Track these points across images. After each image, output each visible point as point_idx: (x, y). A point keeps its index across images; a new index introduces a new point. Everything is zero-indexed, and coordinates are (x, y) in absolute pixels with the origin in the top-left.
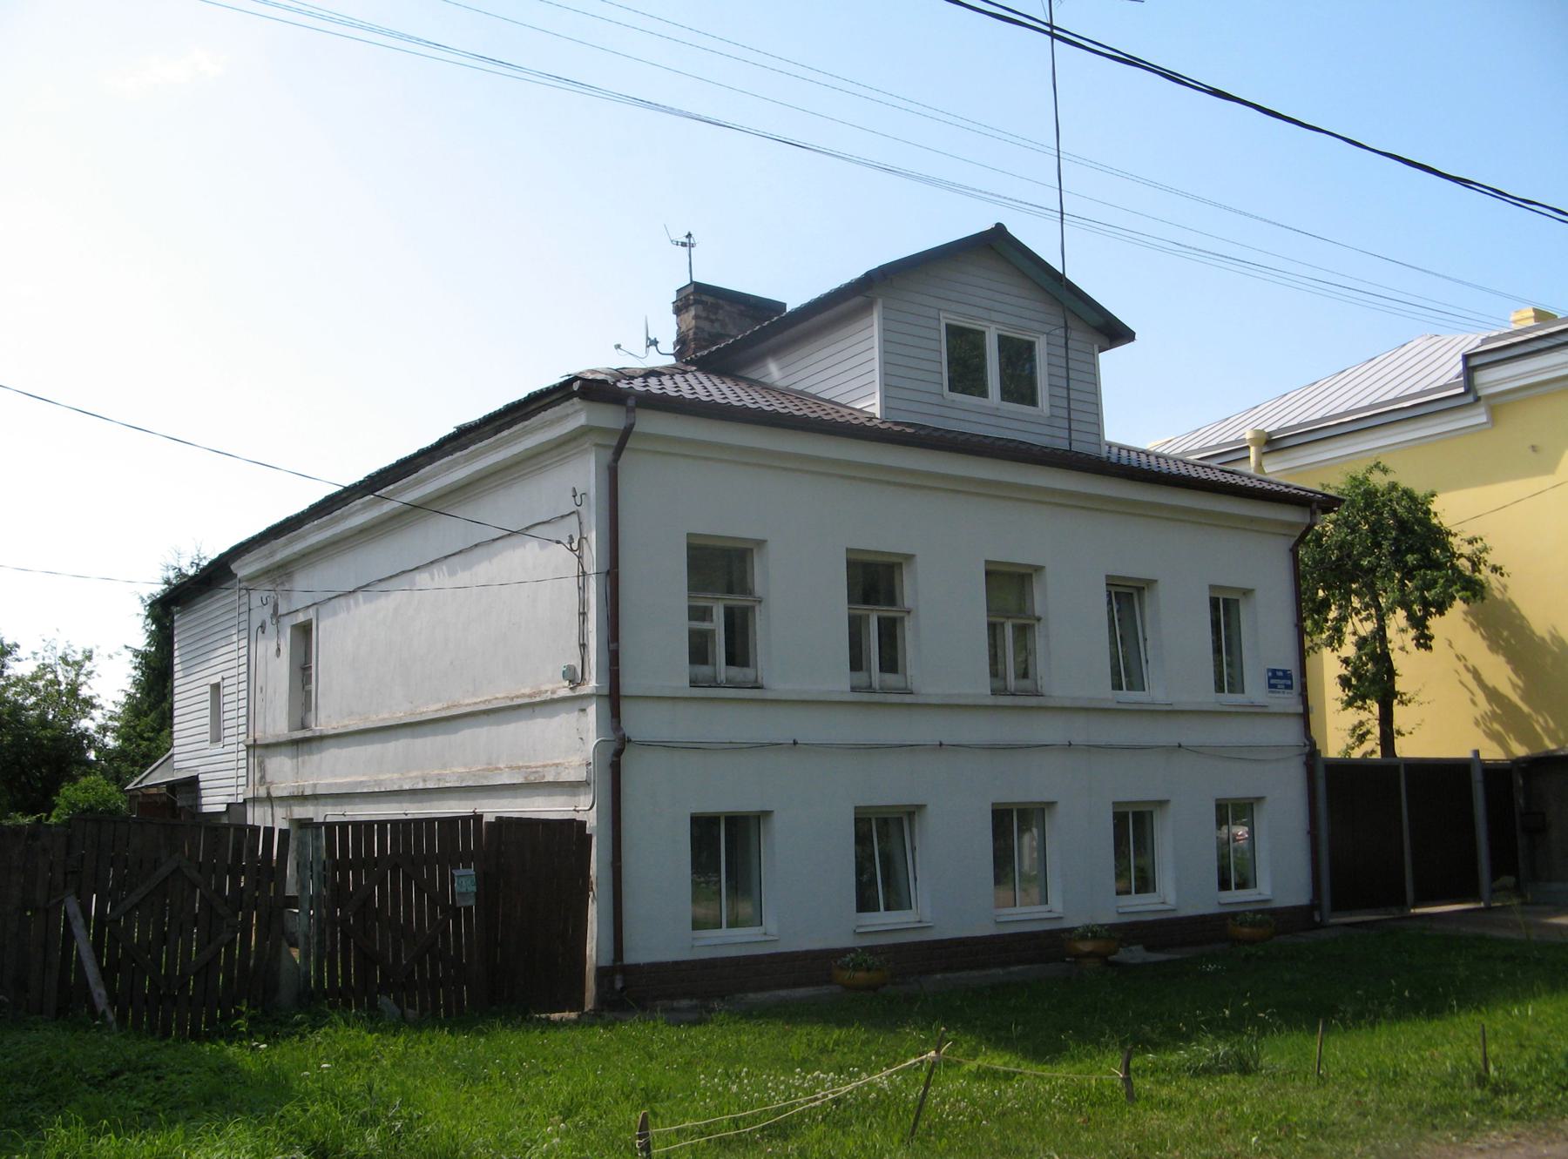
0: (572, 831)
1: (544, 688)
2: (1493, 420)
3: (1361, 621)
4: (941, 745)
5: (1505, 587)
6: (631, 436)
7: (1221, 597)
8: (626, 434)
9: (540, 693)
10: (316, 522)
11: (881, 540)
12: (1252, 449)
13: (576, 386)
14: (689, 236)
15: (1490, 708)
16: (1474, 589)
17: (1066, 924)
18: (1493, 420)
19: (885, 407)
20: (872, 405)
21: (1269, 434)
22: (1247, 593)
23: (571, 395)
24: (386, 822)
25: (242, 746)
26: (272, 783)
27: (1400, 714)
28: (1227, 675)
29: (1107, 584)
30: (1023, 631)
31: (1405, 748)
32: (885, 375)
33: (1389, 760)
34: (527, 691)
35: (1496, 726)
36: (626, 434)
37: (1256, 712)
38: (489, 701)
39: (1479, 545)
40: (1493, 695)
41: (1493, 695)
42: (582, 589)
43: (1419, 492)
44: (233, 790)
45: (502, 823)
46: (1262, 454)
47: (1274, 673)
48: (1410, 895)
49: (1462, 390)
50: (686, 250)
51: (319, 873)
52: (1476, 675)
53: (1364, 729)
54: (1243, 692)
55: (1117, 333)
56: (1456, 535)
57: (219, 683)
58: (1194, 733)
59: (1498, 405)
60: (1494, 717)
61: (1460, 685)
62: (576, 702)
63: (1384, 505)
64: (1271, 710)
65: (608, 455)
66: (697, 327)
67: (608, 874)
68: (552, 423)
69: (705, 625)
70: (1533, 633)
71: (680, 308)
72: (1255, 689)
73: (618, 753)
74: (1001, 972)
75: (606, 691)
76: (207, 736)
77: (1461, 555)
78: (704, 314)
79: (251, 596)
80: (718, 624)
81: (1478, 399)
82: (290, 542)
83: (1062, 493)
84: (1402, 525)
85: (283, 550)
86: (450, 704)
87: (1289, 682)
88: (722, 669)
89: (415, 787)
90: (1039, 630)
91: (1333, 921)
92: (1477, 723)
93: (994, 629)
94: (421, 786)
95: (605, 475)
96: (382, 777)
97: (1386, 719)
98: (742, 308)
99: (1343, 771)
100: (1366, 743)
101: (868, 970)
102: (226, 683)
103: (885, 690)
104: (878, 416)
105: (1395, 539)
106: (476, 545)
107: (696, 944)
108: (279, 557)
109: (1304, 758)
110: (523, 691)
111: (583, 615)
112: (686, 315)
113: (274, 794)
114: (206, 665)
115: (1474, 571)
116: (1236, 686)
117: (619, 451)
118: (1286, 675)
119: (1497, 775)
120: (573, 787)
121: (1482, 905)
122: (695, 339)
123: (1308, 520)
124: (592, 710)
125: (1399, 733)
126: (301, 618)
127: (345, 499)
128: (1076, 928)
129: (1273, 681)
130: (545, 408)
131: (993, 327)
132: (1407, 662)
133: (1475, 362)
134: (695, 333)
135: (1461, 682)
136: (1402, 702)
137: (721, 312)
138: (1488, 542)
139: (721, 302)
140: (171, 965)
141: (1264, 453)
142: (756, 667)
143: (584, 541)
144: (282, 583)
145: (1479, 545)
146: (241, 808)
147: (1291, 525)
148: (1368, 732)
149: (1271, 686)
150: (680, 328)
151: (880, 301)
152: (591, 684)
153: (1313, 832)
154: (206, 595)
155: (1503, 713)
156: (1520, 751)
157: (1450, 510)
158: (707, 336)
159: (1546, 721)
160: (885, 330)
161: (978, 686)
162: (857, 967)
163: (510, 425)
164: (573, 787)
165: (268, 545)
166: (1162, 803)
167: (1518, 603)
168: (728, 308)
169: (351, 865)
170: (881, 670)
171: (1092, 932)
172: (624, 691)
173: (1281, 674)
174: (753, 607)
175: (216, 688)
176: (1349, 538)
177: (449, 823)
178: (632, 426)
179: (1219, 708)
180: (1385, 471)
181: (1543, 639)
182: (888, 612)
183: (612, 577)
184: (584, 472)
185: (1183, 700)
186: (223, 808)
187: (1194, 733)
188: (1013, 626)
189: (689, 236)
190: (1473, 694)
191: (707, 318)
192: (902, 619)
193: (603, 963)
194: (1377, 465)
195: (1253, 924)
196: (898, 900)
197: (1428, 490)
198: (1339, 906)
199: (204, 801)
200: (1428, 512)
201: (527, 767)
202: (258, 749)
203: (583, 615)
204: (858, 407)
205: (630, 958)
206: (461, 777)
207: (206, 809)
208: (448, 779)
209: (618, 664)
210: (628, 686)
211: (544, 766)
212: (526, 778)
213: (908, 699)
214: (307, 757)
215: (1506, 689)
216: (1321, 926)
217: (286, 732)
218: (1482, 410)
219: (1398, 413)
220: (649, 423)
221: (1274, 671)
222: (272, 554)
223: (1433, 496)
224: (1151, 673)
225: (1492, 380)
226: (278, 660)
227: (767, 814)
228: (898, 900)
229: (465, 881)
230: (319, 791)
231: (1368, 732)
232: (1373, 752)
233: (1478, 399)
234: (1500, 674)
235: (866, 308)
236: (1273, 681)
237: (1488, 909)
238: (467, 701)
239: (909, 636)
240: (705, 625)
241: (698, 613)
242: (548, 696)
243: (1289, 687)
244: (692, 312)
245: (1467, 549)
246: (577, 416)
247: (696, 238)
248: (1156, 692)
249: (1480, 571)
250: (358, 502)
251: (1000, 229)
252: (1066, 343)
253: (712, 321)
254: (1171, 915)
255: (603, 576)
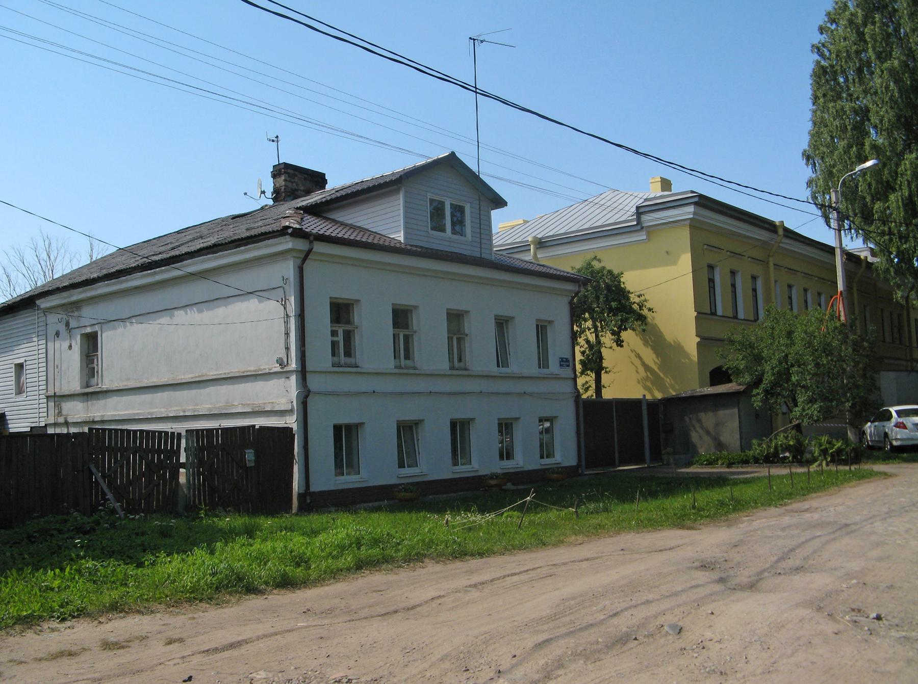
0: (288, 431)
1: (262, 367)
2: (649, 238)
3: (591, 333)
4: (525, 393)
5: (654, 318)
6: (311, 254)
7: (540, 324)
8: (309, 252)
9: (261, 370)
10: (106, 282)
11: (405, 300)
12: (532, 246)
13: (290, 231)
14: (277, 137)
15: (645, 374)
16: (642, 318)
17: (480, 473)
18: (649, 238)
19: (405, 238)
20: (400, 237)
21: (540, 239)
22: (551, 322)
23: (287, 234)
24: (204, 430)
25: (43, 396)
26: (67, 415)
27: (604, 377)
28: (543, 362)
29: (495, 319)
30: (459, 340)
31: (607, 394)
32: (406, 223)
33: (599, 399)
34: (252, 369)
35: (649, 384)
36: (309, 252)
37: (555, 377)
38: (228, 373)
39: (642, 298)
40: (647, 368)
41: (647, 368)
42: (286, 323)
43: (616, 272)
44: (37, 420)
45: (262, 429)
46: (536, 249)
47: (562, 360)
48: (617, 461)
49: (635, 223)
50: (275, 143)
51: (194, 453)
52: (638, 356)
53: (588, 385)
54: (548, 368)
55: (499, 202)
56: (632, 293)
57: (23, 363)
58: (529, 387)
59: (651, 231)
60: (647, 378)
61: (631, 364)
62: (284, 374)
63: (601, 278)
64: (562, 376)
65: (299, 262)
66: (285, 186)
67: (302, 452)
68: (272, 245)
69: (335, 339)
70: (665, 340)
71: (275, 175)
72: (554, 367)
73: (306, 397)
74: (455, 495)
75: (300, 369)
76: (13, 391)
77: (634, 303)
78: (288, 179)
79: (47, 318)
80: (340, 338)
81: (642, 228)
82: (85, 291)
83: (482, 278)
84: (608, 287)
85: (77, 295)
86: (200, 374)
87: (568, 364)
88: (343, 359)
89: (178, 415)
90: (467, 340)
91: (585, 473)
92: (639, 382)
93: (450, 339)
94: (182, 414)
95: (297, 270)
96: (152, 411)
97: (598, 380)
98: (306, 176)
99: (588, 403)
100: (589, 392)
101: (411, 492)
102: (28, 363)
103: (407, 368)
104: (402, 241)
105: (606, 295)
106: (217, 299)
107: (337, 482)
108: (74, 298)
109: (574, 398)
110: (249, 369)
111: (287, 334)
112: (279, 179)
113: (70, 420)
114: (11, 353)
115: (640, 310)
116: (546, 366)
117: (304, 260)
118: (567, 360)
119: (653, 406)
120: (282, 413)
121: (646, 466)
122: (285, 192)
123: (577, 289)
124: (293, 378)
125: (604, 387)
126: (89, 330)
127: (129, 272)
128: (487, 475)
129: (562, 363)
130: (264, 239)
131: (448, 200)
132: (610, 355)
133: (641, 210)
134: (285, 189)
135: (632, 363)
136: (606, 372)
137: (296, 178)
138: (647, 297)
139: (296, 173)
140: (134, 494)
141: (537, 248)
142: (355, 357)
143: (287, 301)
144: (72, 312)
145: (642, 298)
146: (44, 429)
147: (570, 291)
148: (590, 386)
149: (561, 365)
150: (275, 185)
151: (403, 188)
152: (293, 365)
153: (578, 432)
154: (11, 315)
155: (653, 378)
156: (659, 396)
157: (632, 281)
158: (290, 190)
159: (671, 381)
160: (405, 202)
161: (445, 366)
162: (406, 491)
163: (246, 245)
164: (282, 413)
165: (67, 292)
166: (517, 419)
167: (659, 325)
168: (299, 176)
169: (150, 451)
170: (344, 356)
171: (493, 476)
172: (308, 369)
173: (565, 360)
174: (354, 331)
175: (20, 367)
176: (586, 293)
177: (243, 429)
178: (312, 249)
179: (540, 376)
180: (599, 261)
181: (670, 343)
182: (407, 332)
183: (301, 317)
184: (288, 269)
185: (526, 372)
186: (28, 429)
187: (529, 387)
188: (457, 338)
189: (277, 137)
190: (636, 367)
191: (290, 181)
192: (413, 335)
193: (301, 492)
194: (595, 258)
195: (558, 473)
196: (414, 464)
197: (620, 271)
198: (589, 466)
199: (10, 426)
200: (620, 282)
201: (253, 404)
202: (57, 398)
203: (287, 334)
204: (391, 237)
205: (314, 488)
206: (210, 409)
207: (11, 431)
208: (200, 410)
209: (305, 357)
210: (310, 367)
211: (265, 404)
212: (253, 409)
213: (417, 372)
214: (95, 402)
215: (652, 365)
216: (580, 475)
217: (79, 388)
218: (644, 233)
219: (601, 233)
220: (319, 247)
221: (562, 359)
222: (72, 295)
223: (622, 274)
224: (511, 359)
225: (648, 220)
226: (70, 352)
227: (362, 424)
228: (414, 464)
229: (250, 456)
230: (105, 419)
231: (590, 386)
232: (592, 396)
233: (642, 228)
234: (649, 356)
235: (397, 191)
236: (562, 363)
237: (649, 467)
238: (212, 373)
239: (415, 343)
240: (335, 339)
241: (334, 333)
242: (267, 371)
243: (568, 366)
244: (283, 178)
245: (637, 300)
246: (287, 243)
247: (280, 138)
248: (514, 368)
249: (643, 310)
250: (138, 274)
251: (453, 154)
252: (480, 208)
253: (292, 182)
254: (522, 470)
255: (297, 317)
